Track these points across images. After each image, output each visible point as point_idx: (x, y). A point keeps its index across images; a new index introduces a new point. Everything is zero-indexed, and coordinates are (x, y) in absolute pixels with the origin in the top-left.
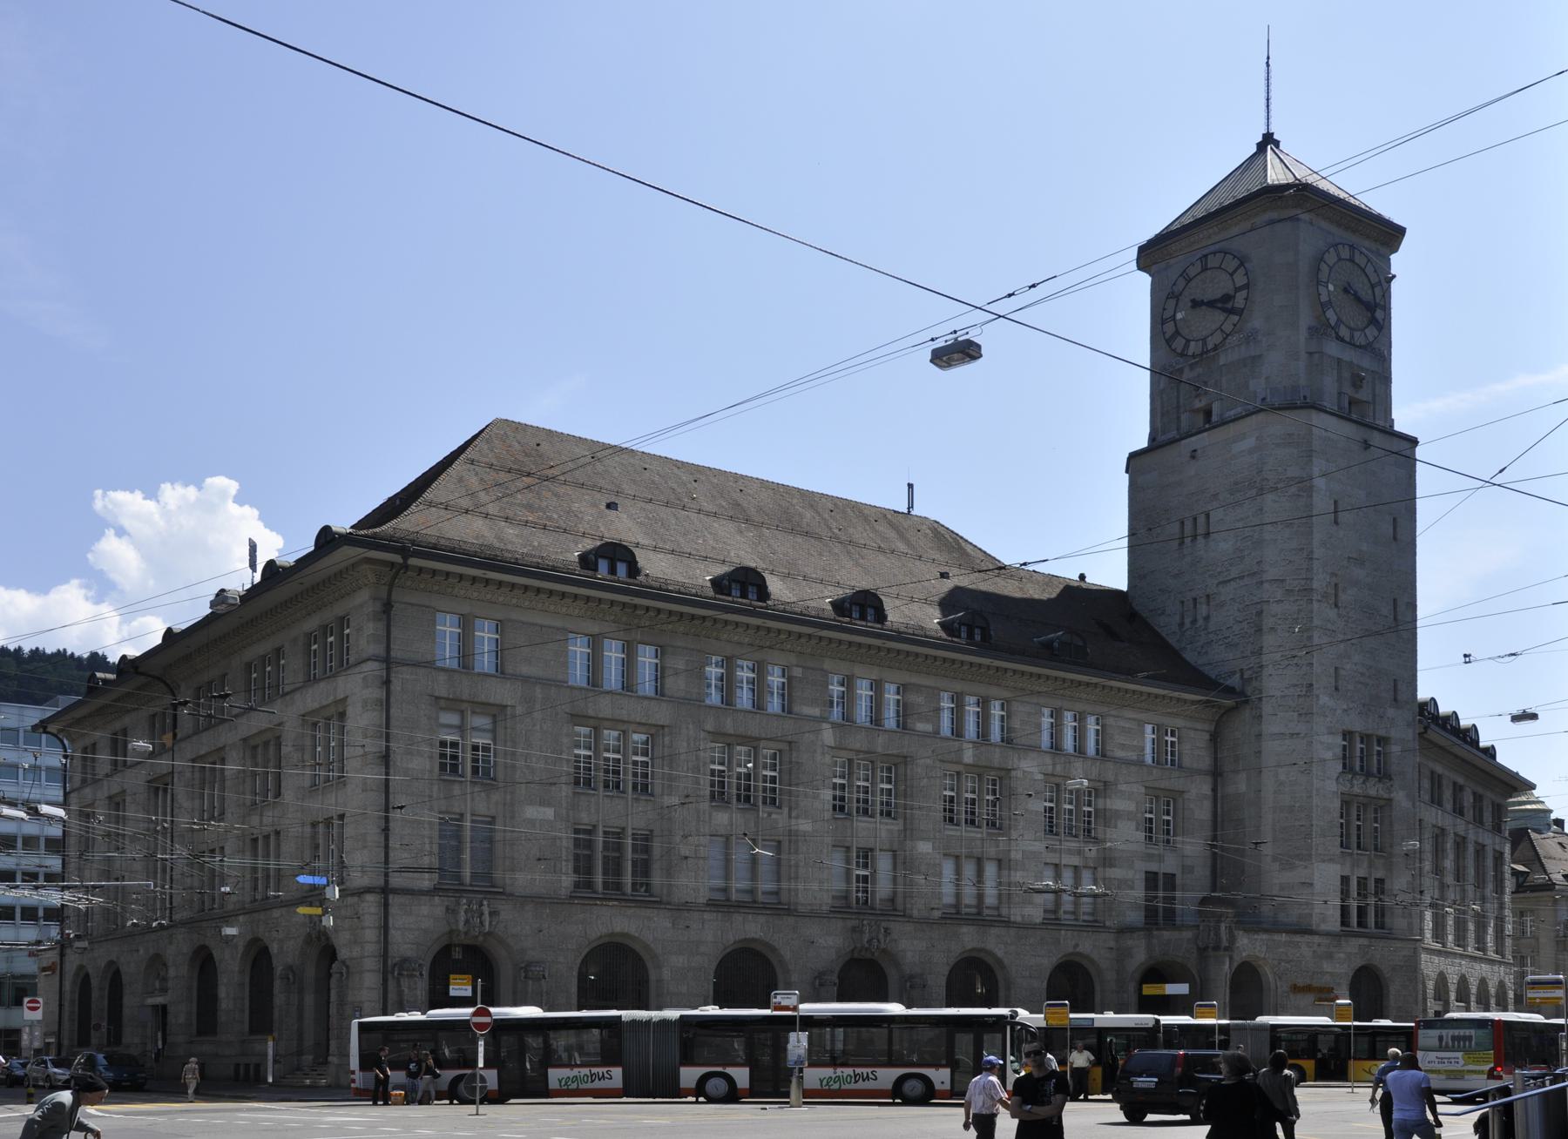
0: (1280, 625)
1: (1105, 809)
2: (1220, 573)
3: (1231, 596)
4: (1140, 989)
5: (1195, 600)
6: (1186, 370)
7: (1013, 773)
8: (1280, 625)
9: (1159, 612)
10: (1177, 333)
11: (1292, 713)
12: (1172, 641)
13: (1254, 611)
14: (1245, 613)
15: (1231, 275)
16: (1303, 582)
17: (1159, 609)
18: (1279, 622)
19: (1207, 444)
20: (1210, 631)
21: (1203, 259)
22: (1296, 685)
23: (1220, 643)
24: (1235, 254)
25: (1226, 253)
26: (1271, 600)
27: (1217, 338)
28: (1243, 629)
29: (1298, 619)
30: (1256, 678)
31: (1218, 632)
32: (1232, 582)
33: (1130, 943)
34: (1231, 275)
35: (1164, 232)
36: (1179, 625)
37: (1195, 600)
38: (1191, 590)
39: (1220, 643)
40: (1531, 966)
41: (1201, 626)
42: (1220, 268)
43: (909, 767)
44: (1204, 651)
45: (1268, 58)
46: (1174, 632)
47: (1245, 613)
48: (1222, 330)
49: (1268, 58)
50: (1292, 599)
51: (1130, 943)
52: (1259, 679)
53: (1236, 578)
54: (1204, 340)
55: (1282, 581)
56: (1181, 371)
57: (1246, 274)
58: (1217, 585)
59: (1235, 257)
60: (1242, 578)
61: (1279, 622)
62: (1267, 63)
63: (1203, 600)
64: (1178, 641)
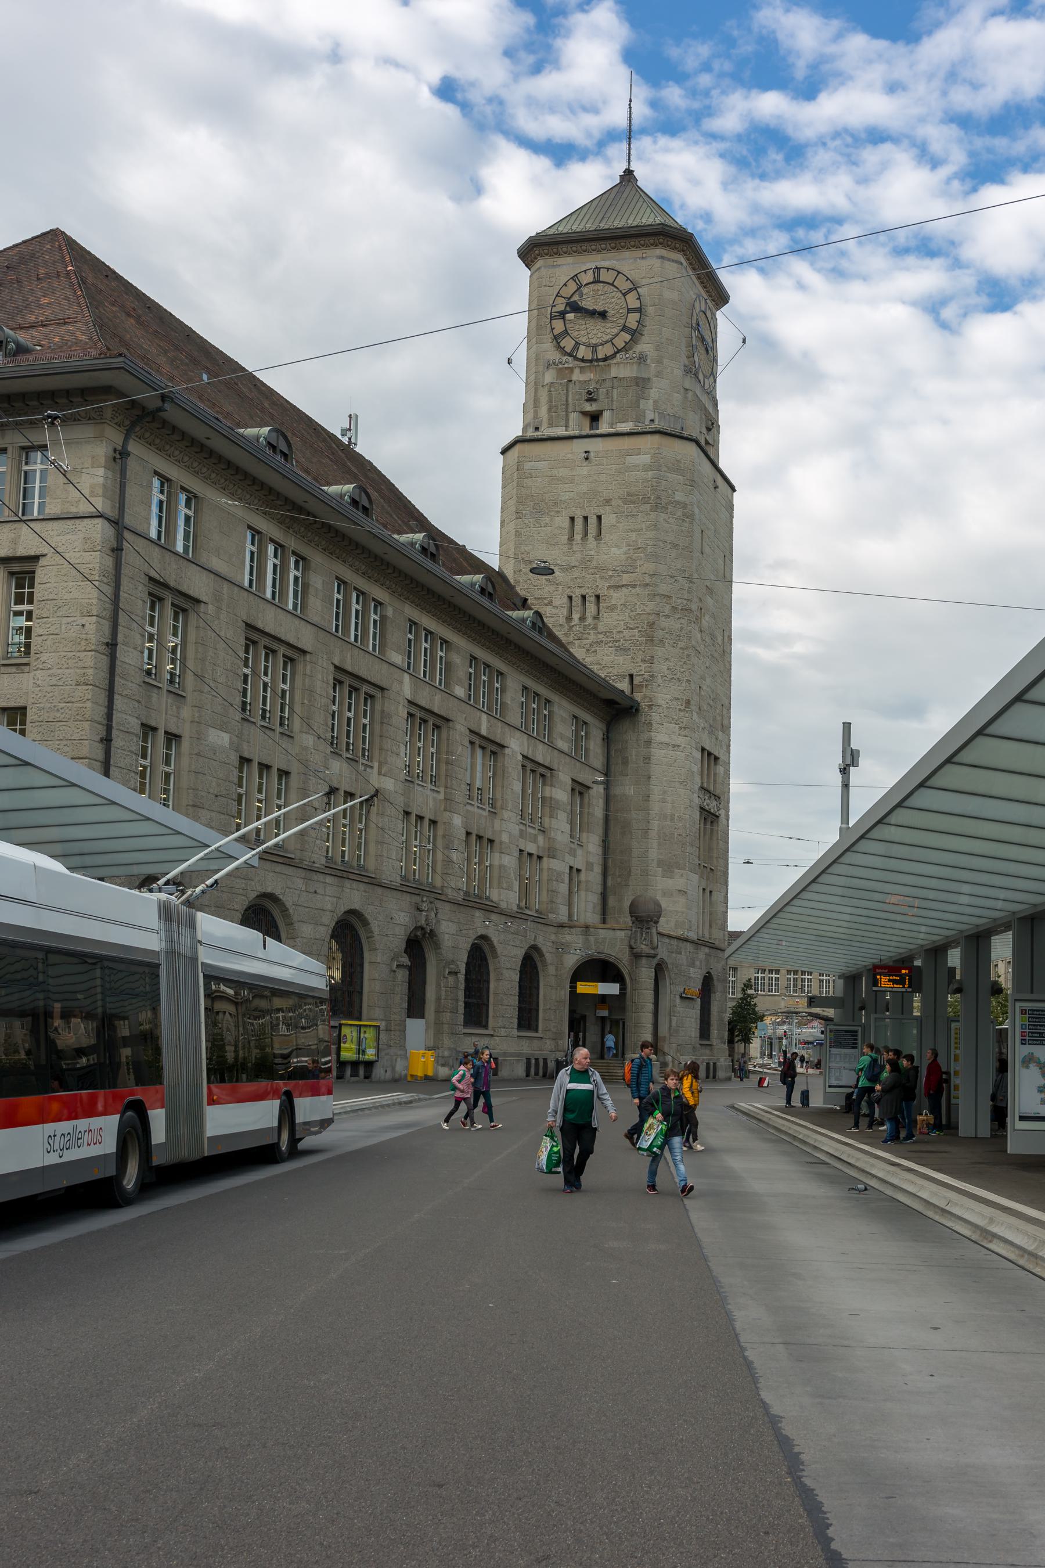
0: (667, 639)
1: (551, 798)
2: (611, 576)
3: (622, 602)
4: (623, 989)
5: (584, 597)
6: (577, 371)
7: (507, 751)
8: (667, 639)
9: (546, 602)
10: (566, 333)
11: (675, 725)
12: (559, 633)
13: (646, 622)
14: (636, 621)
15: (624, 295)
16: (685, 602)
17: (545, 599)
18: (667, 636)
19: (601, 449)
20: (600, 631)
21: (596, 271)
22: (678, 699)
23: (611, 644)
24: (629, 277)
25: (619, 273)
26: (661, 614)
27: (608, 350)
28: (634, 636)
29: (680, 636)
30: (646, 686)
31: (608, 634)
32: (623, 588)
33: (568, 938)
34: (624, 295)
35: (551, 232)
36: (567, 618)
37: (584, 597)
38: (580, 587)
39: (611, 644)
40: (805, 979)
41: (590, 625)
42: (612, 284)
43: (451, 732)
44: (593, 649)
45: (630, 101)
46: (561, 625)
47: (636, 621)
48: (613, 344)
49: (630, 101)
50: (677, 616)
51: (568, 938)
52: (649, 687)
53: (629, 585)
54: (595, 347)
55: (670, 597)
56: (571, 370)
57: (639, 298)
58: (609, 587)
59: (628, 279)
60: (634, 586)
61: (667, 636)
62: (630, 105)
63: (593, 599)
64: (566, 634)
